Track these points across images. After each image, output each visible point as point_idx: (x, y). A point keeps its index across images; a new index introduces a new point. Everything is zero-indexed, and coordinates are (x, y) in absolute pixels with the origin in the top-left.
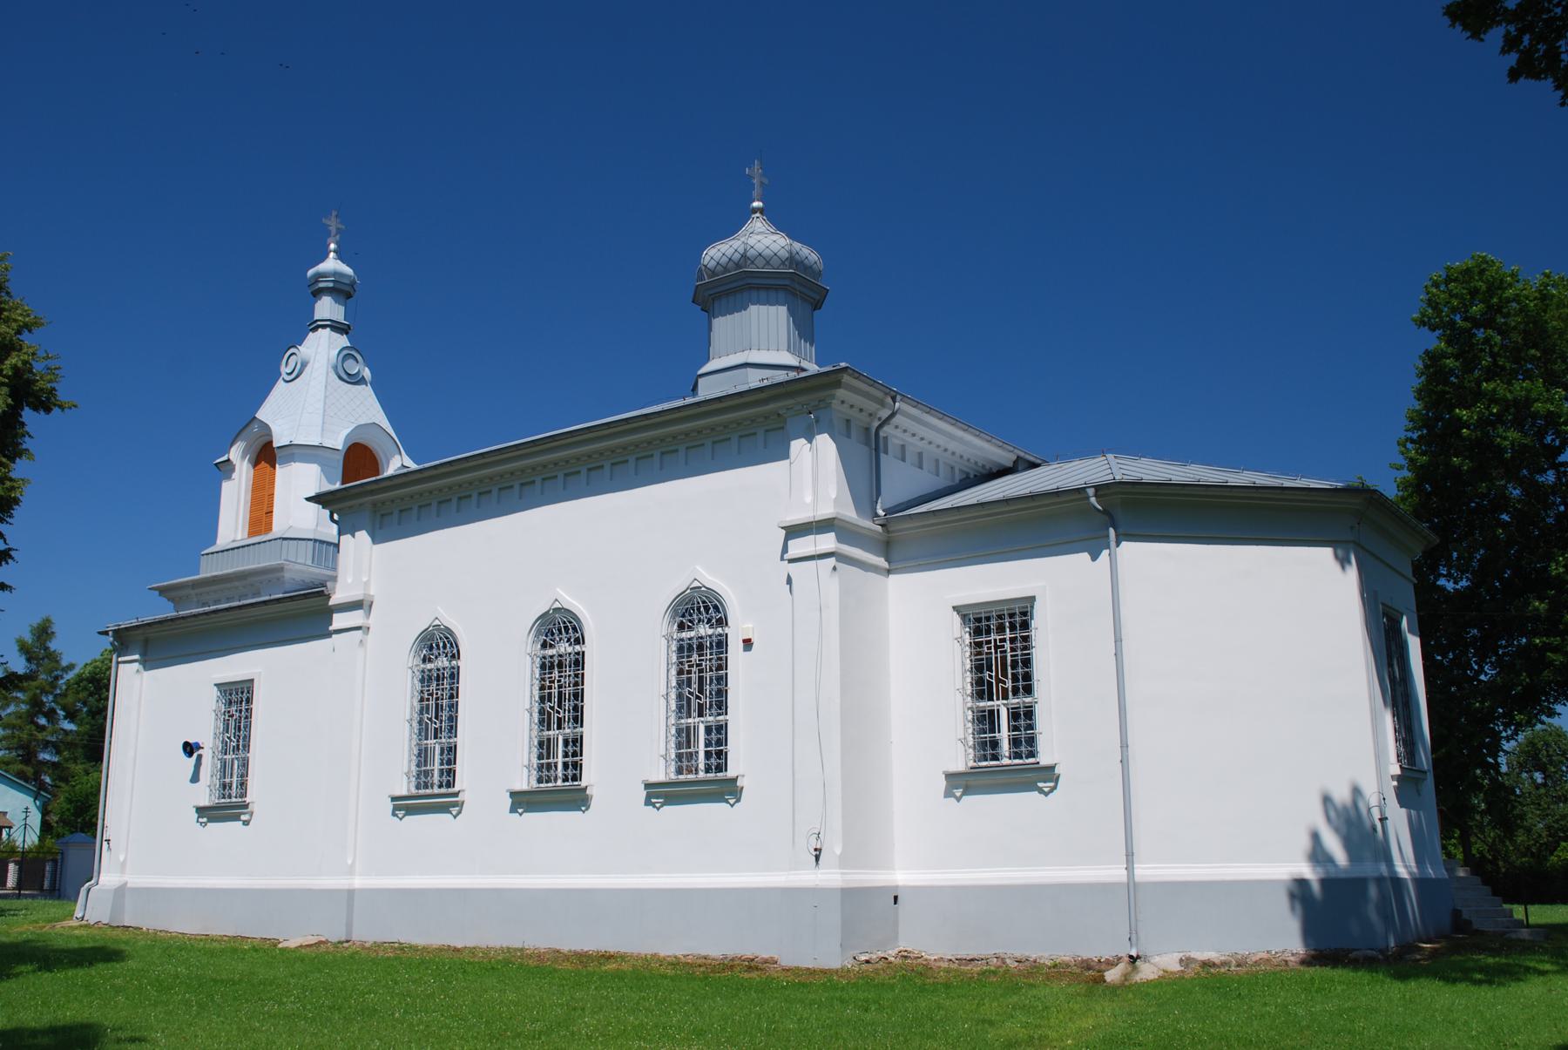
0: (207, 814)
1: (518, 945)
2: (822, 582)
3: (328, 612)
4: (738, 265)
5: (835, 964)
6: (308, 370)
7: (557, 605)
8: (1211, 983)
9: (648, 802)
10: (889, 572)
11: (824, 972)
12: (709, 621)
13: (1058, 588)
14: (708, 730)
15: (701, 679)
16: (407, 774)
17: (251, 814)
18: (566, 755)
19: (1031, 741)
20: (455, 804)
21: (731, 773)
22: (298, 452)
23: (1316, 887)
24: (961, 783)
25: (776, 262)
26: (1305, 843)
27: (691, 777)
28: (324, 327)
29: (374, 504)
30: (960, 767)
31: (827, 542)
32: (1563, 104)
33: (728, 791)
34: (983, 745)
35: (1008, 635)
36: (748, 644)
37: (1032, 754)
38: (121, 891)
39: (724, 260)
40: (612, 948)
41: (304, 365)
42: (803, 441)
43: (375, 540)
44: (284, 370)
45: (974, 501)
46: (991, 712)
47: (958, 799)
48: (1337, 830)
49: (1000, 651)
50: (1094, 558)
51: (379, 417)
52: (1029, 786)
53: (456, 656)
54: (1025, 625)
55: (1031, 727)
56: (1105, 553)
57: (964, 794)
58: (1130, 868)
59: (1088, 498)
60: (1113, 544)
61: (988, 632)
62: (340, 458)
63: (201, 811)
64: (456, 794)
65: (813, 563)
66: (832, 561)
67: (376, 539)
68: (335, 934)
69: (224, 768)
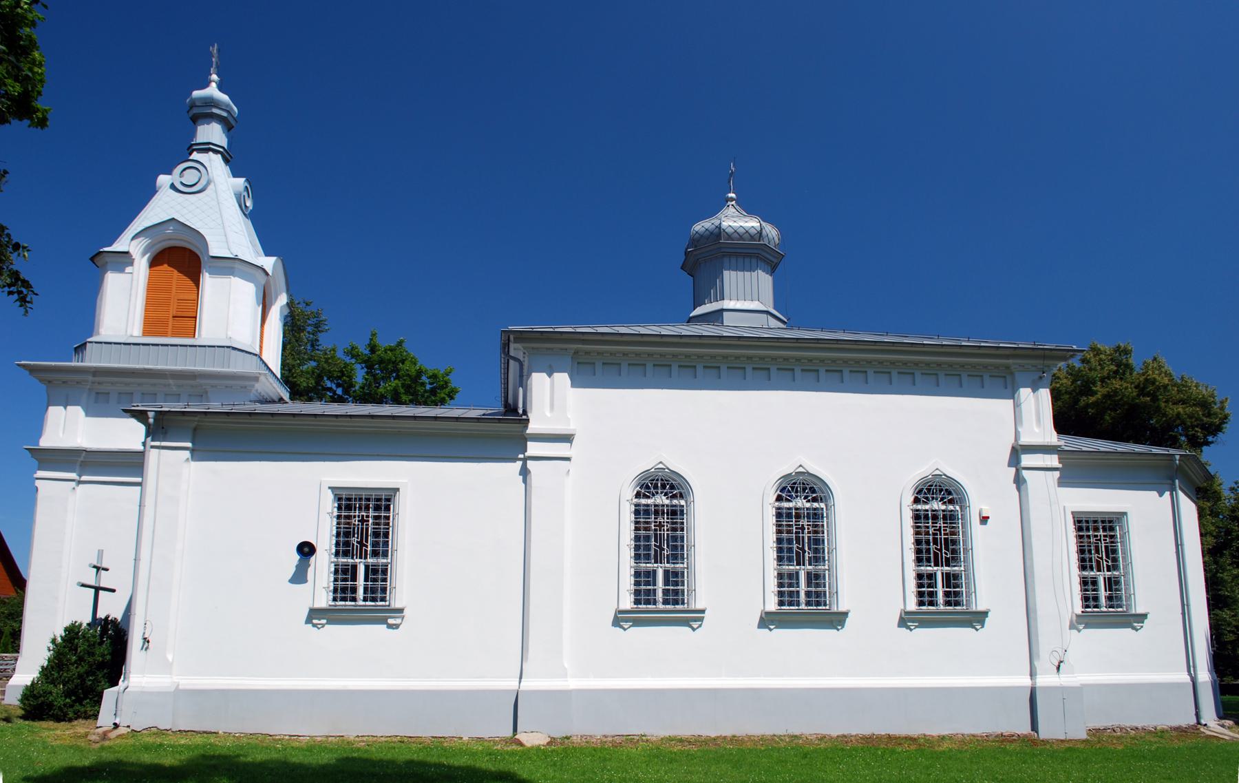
3: (521, 440)
4: (752, 237)
6: (211, 187)
7: (801, 470)
29: (576, 352)
31: (1053, 460)
32: (6, 172)
35: (371, 513)
42: (1029, 390)
43: (575, 384)
45: (366, 413)
49: (1099, 542)
50: (1161, 495)
54: (388, 508)
55: (385, 580)
56: (1167, 494)
58: (1032, 674)
61: (1088, 529)
63: (314, 615)
69: (345, 574)
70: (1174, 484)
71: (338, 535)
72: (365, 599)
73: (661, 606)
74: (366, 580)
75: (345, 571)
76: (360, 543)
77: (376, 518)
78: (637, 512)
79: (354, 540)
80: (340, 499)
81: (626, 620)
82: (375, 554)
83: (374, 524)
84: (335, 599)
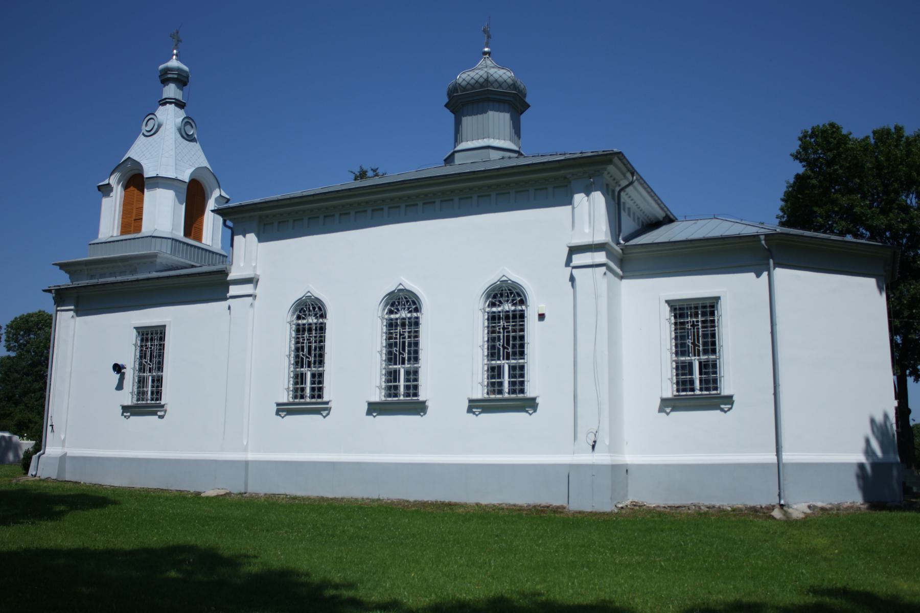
0: (129, 410)
1: (376, 497)
2: (595, 281)
3: (226, 285)
4: (482, 85)
5: (608, 509)
7: (401, 287)
8: (825, 519)
9: (277, 413)
10: (622, 278)
11: (604, 513)
12: (315, 315)
13: (736, 294)
14: (313, 376)
15: (310, 347)
16: (132, 393)
17: (165, 411)
18: (153, 387)
19: (416, 387)
20: (325, 409)
21: (421, 398)
22: (159, 182)
23: (868, 468)
24: (668, 405)
25: (504, 85)
26: (862, 445)
27: (499, 396)
28: (171, 103)
30: (284, 400)
31: (601, 257)
33: (419, 408)
34: (389, 388)
36: (542, 317)
37: (716, 389)
38: (63, 458)
39: (473, 82)
40: (454, 500)
41: (160, 126)
42: (583, 195)
44: (144, 129)
46: (395, 371)
47: (668, 414)
48: (877, 438)
49: (695, 327)
50: (758, 276)
51: (205, 163)
52: (715, 407)
53: (323, 316)
54: (712, 313)
55: (715, 373)
56: (765, 274)
57: (672, 411)
59: (760, 240)
60: (772, 268)
62: (185, 186)
63: (125, 409)
64: (327, 403)
65: (590, 270)
66: (604, 269)
67: (261, 239)
68: (557, 500)
69: (141, 382)
70: (768, 264)
71: (676, 338)
72: (701, 390)
73: (308, 400)
74: (701, 374)
75: (683, 367)
76: (693, 343)
77: (703, 322)
78: (298, 331)
79: (689, 342)
80: (675, 309)
81: (477, 407)
82: (706, 352)
83: (703, 327)
84: (678, 391)
